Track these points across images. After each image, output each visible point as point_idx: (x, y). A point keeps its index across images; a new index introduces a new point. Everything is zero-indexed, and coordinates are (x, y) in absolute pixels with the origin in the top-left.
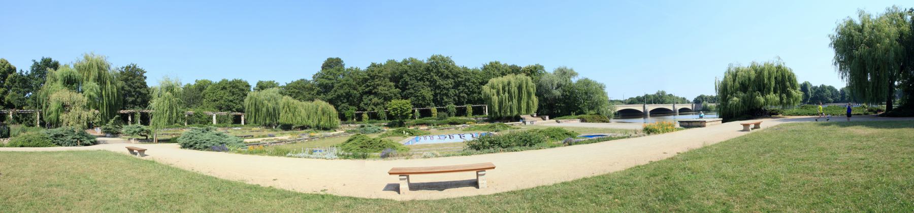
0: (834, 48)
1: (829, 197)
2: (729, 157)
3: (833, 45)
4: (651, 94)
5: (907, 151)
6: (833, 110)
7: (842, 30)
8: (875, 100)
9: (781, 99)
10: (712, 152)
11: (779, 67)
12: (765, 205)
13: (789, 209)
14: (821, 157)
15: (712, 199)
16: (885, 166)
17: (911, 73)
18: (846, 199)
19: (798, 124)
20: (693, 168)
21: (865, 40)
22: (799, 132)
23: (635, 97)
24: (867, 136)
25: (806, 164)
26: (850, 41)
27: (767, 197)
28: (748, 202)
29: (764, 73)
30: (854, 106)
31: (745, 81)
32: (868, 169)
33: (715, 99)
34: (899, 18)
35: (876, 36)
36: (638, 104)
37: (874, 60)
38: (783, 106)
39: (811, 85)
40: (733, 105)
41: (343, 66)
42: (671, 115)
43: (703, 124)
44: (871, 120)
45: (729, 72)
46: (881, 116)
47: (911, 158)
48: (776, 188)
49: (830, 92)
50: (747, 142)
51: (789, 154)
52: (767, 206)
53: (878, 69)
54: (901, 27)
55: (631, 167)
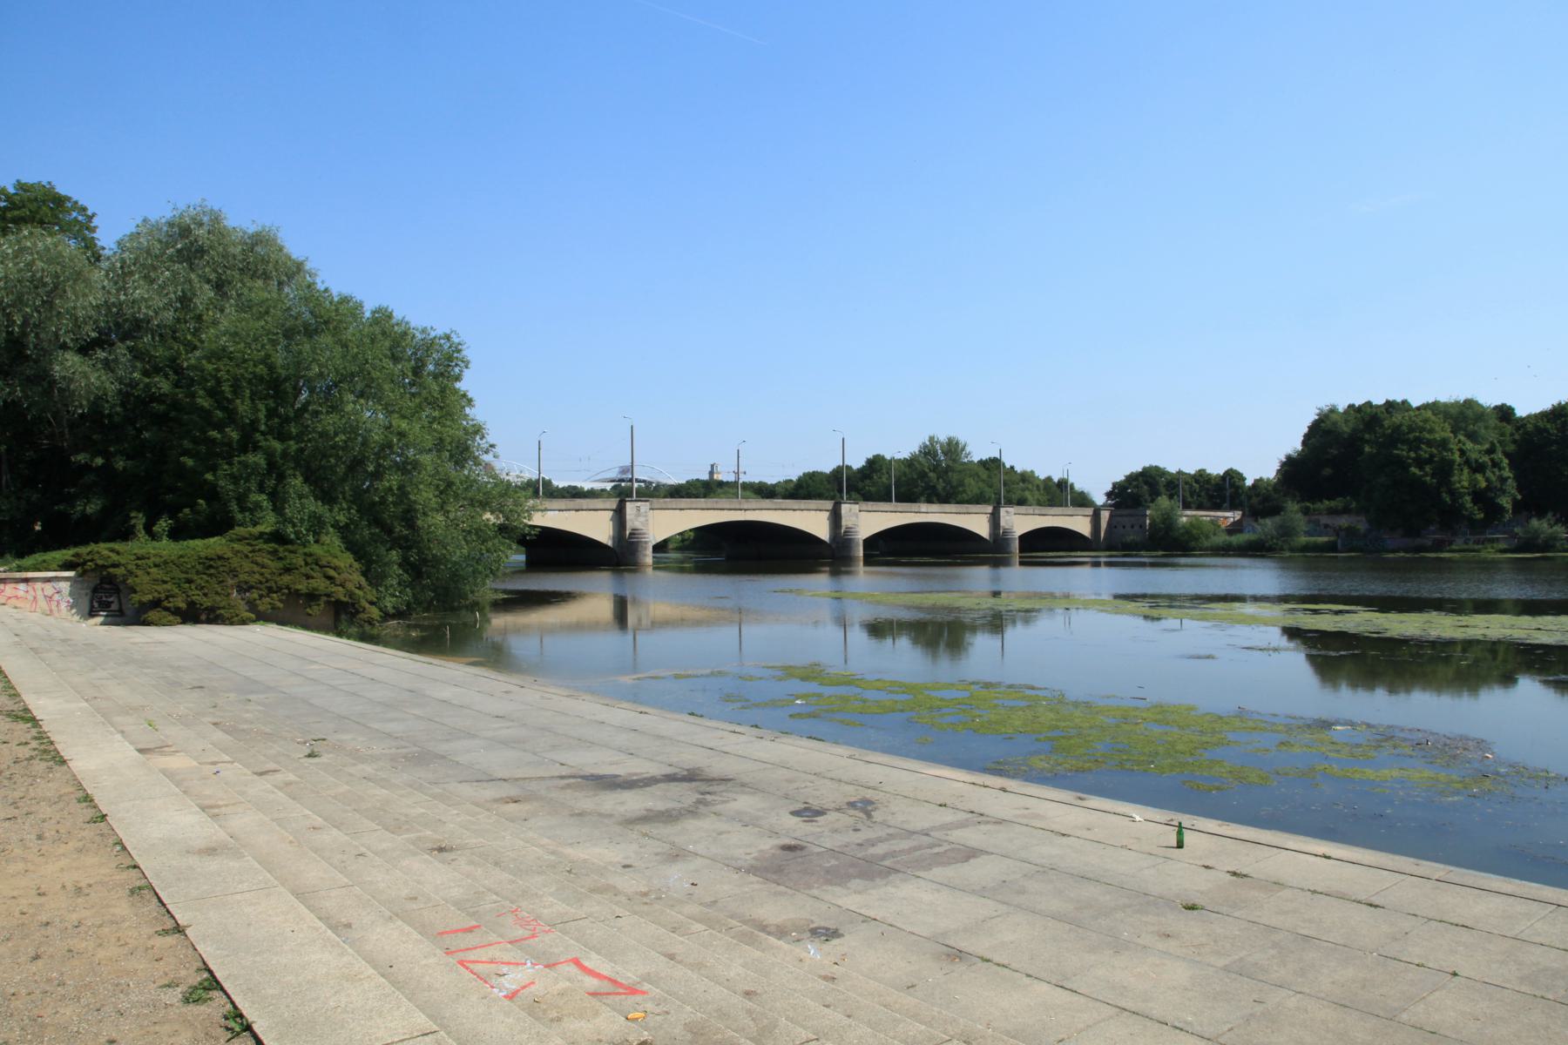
41: (83, 229)
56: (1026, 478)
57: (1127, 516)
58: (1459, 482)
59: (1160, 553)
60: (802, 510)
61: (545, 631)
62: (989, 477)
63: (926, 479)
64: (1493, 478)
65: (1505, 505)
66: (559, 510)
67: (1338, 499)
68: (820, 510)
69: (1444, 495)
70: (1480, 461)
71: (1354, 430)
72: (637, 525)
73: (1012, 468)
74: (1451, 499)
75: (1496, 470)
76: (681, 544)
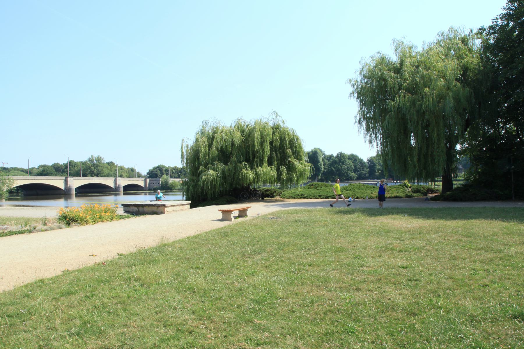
0: (357, 98)
1: (351, 324)
2: (199, 259)
3: (356, 95)
4: (79, 161)
5: (481, 257)
6: (356, 190)
7: (369, 71)
8: (424, 174)
9: (279, 174)
10: (174, 253)
11: (276, 128)
12: (252, 334)
13: (289, 340)
14: (338, 262)
15: (172, 325)
16: (443, 280)
17: (484, 129)
18: (378, 329)
19: (305, 211)
20: (143, 277)
21: (405, 84)
22: (305, 223)
23: (50, 163)
24: (411, 232)
25: (315, 272)
26: (382, 87)
27: (256, 321)
28: (228, 329)
29: (254, 136)
30: (389, 185)
31: (226, 146)
32: (414, 283)
33: (181, 172)
34: (461, 45)
35: (422, 77)
36: (56, 175)
37: (421, 113)
38: (282, 184)
39: (324, 154)
40: (208, 182)
42: (59, 198)
43: (161, 209)
44: (417, 206)
45: (202, 133)
46: (433, 199)
47: (487, 271)
48: (271, 308)
49: (351, 164)
50: (227, 238)
51: (291, 256)
52: (256, 335)
53: (428, 126)
54: (463, 58)
55: (26, 283)
56: (122, 168)
59: (164, 191)
62: (111, 168)
63: (90, 169)
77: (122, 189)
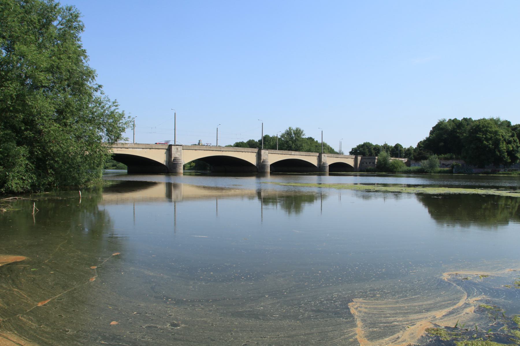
57: (367, 159)
58: (503, 147)
60: (245, 152)
61: (135, 201)
64: (514, 146)
65: (519, 157)
66: (142, 148)
67: (447, 154)
68: (253, 152)
69: (497, 152)
70: (510, 139)
71: (454, 129)
72: (177, 156)
73: (317, 141)
74: (500, 154)
75: (515, 143)
76: (190, 168)
77: (328, 169)
